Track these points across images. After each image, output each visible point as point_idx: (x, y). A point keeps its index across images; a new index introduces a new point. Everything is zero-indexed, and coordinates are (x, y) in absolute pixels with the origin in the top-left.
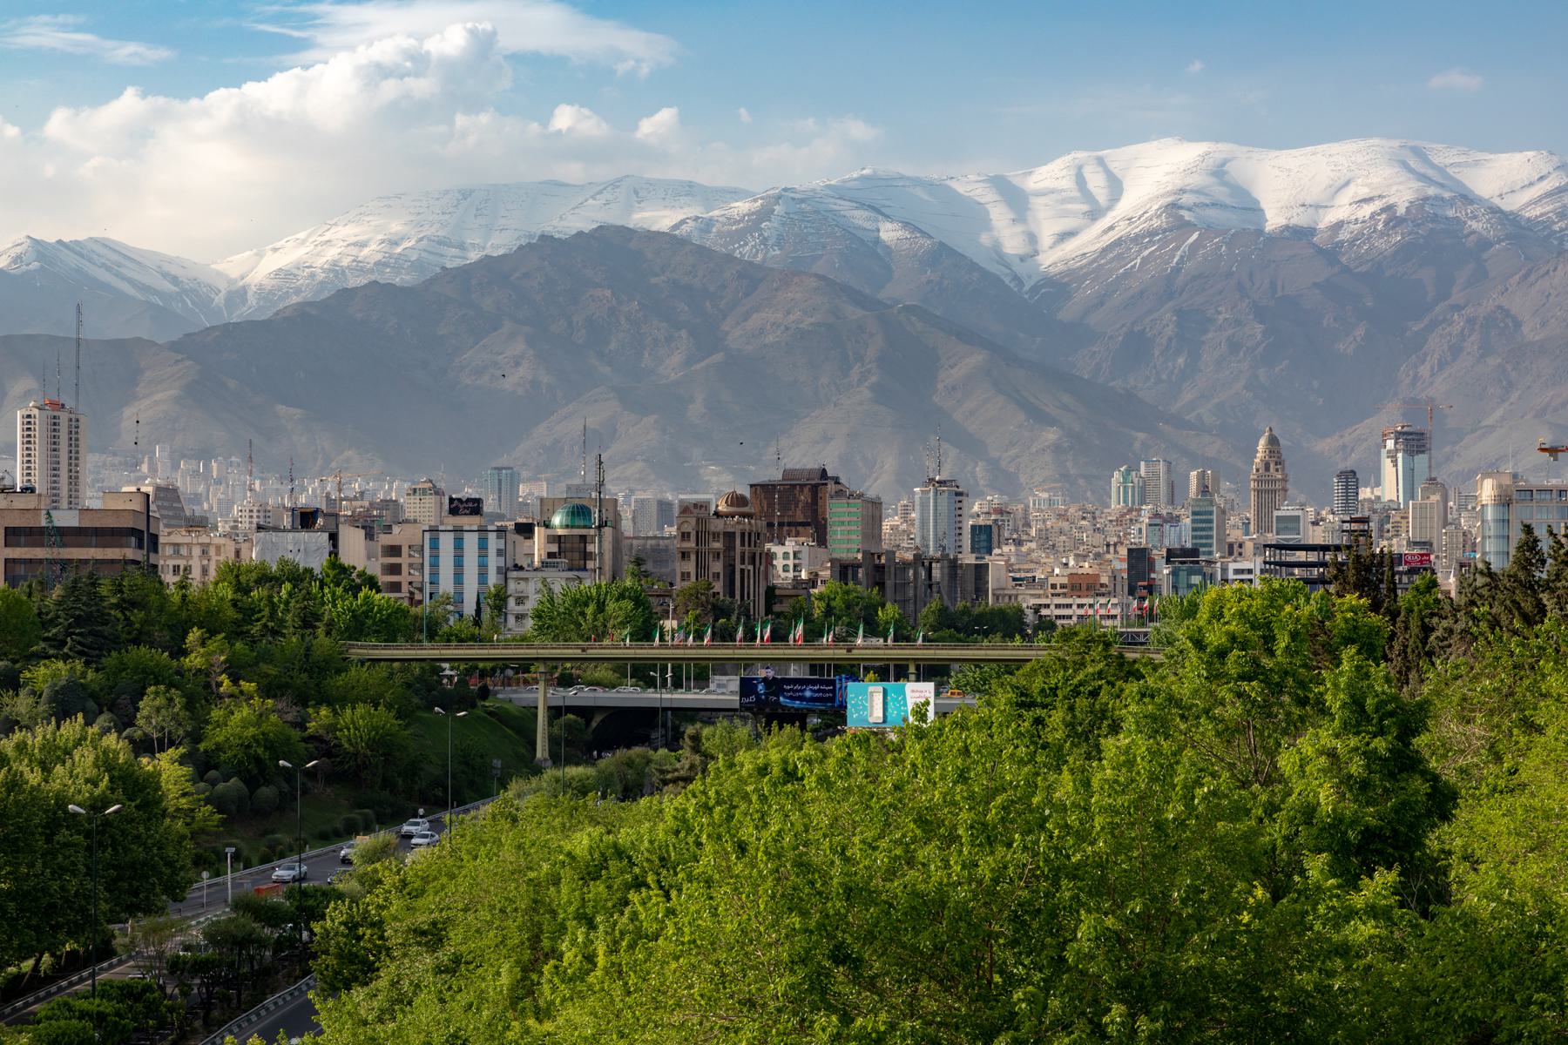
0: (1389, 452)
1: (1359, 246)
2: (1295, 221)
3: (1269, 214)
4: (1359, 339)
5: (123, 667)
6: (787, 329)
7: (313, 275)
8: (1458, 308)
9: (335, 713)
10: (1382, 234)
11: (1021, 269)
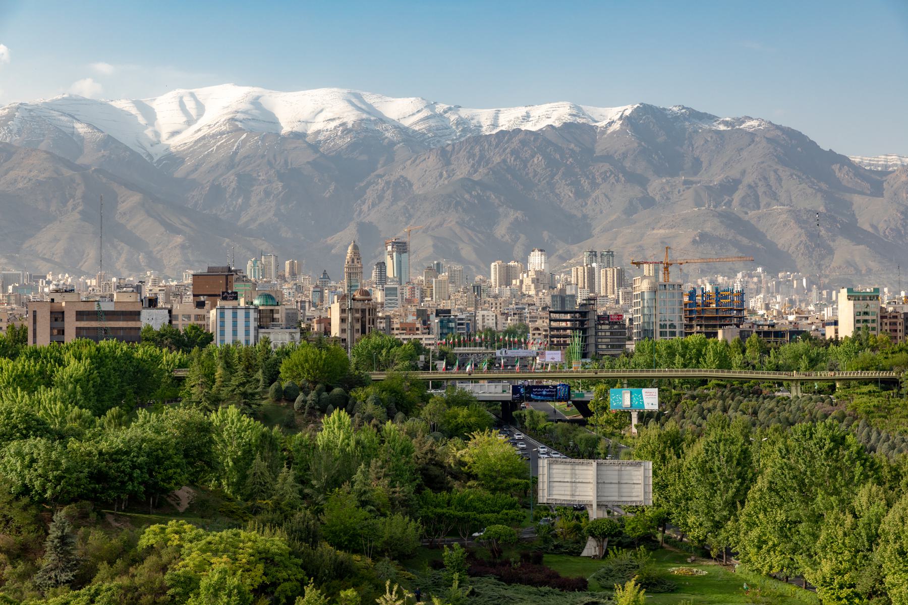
1: (329, 143)
2: (295, 129)
6: (30, 180)
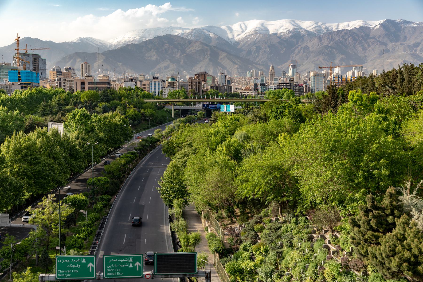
2: (274, 32)
3: (270, 31)
5: (113, 103)
7: (122, 42)
8: (300, 46)
9: (145, 110)
11: (232, 40)
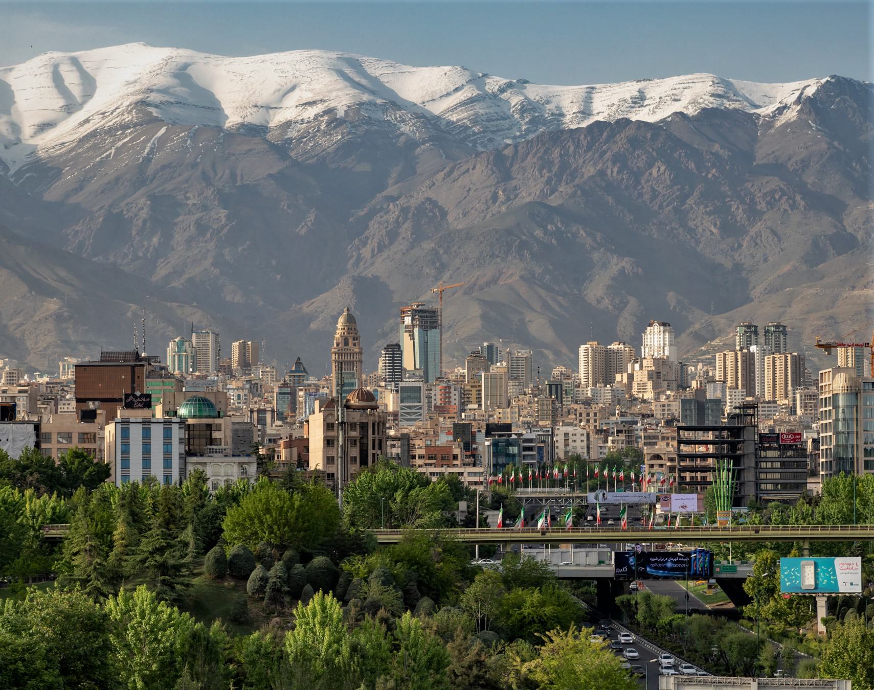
0: (407, 327)
1: (305, 143)
4: (309, 224)
8: (392, 199)
10: (325, 133)
